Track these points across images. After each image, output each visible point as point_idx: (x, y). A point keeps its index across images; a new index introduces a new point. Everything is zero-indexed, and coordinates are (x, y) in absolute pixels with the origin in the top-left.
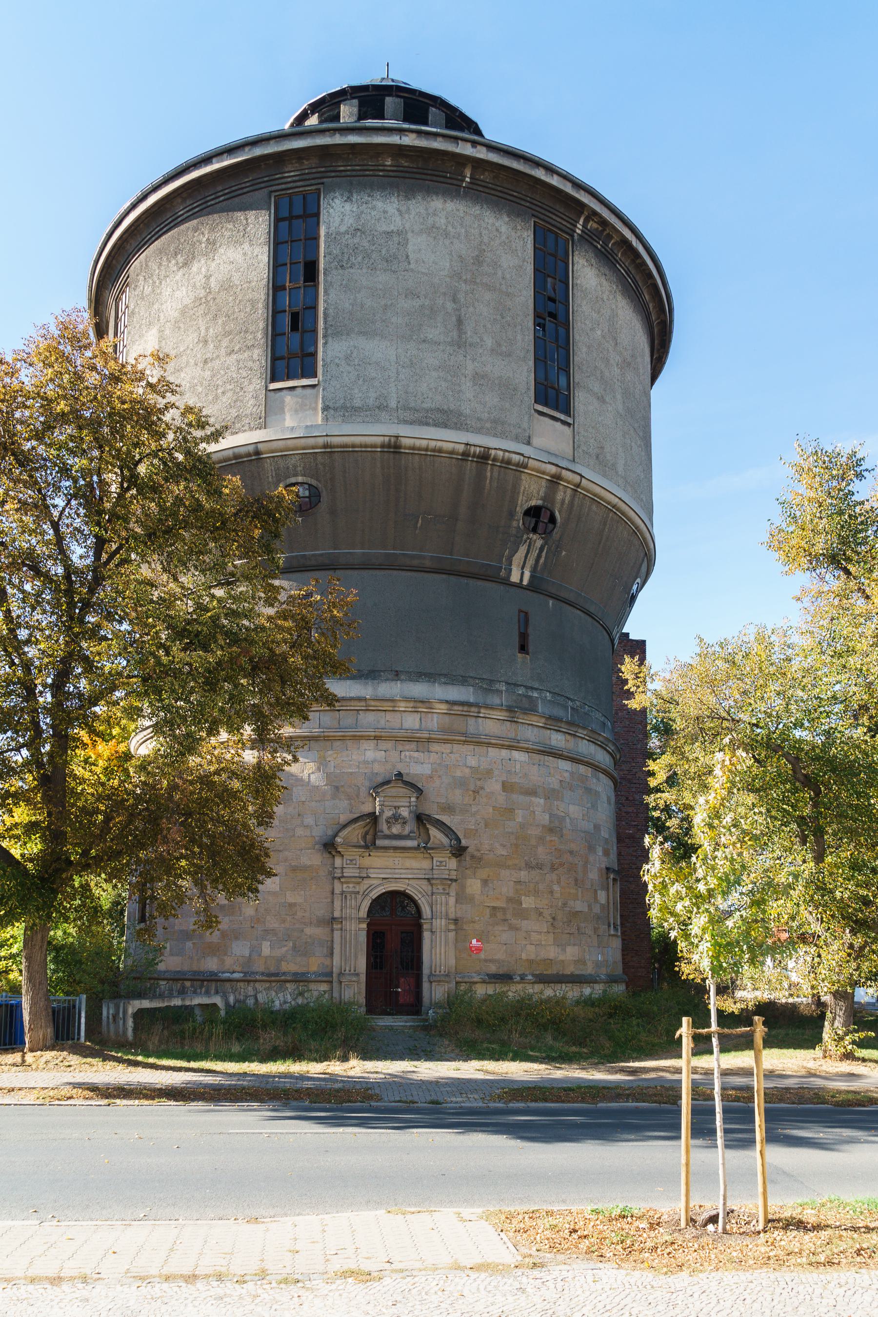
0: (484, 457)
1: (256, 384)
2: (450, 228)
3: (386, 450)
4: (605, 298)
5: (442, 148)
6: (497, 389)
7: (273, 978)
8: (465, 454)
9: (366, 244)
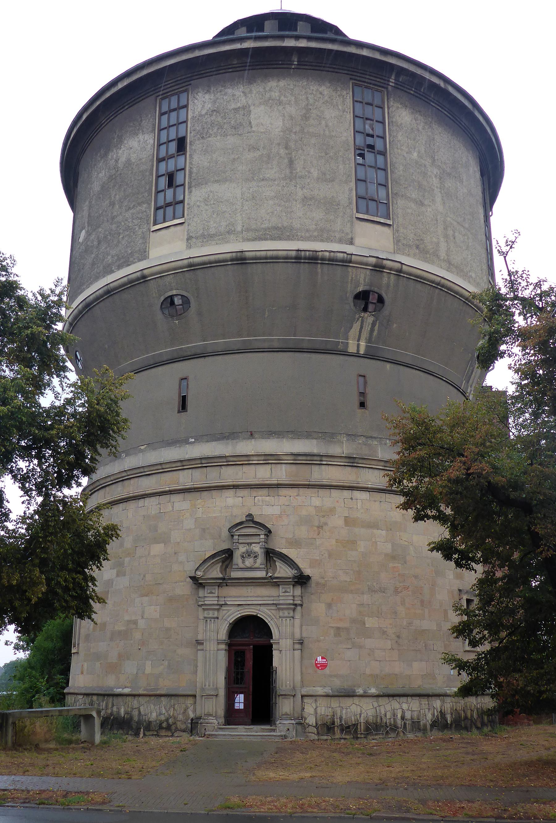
2: (282, 98)
9: (219, 119)
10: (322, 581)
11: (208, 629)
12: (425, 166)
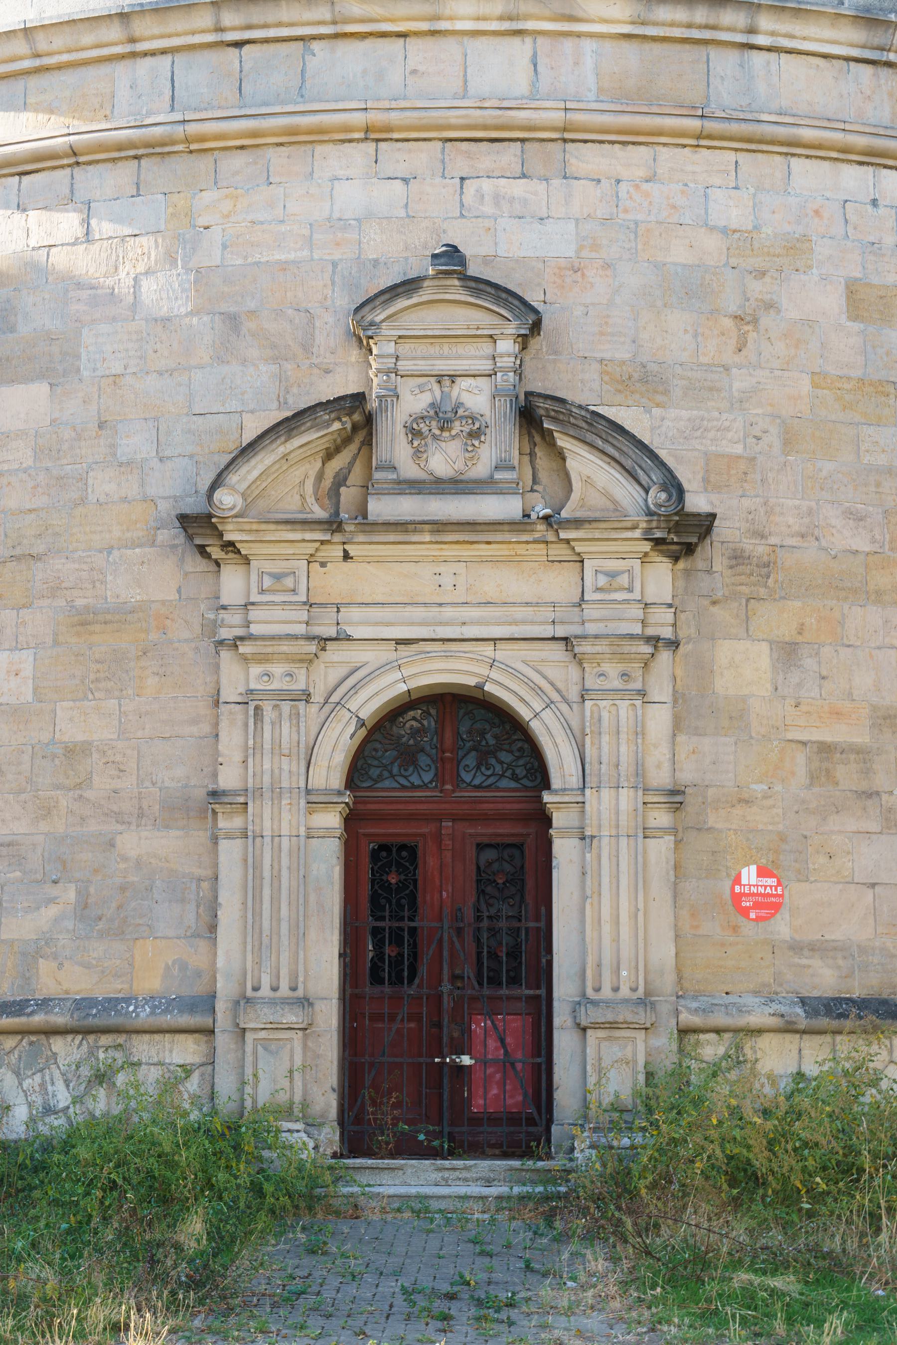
10: (760, 550)
11: (267, 746)
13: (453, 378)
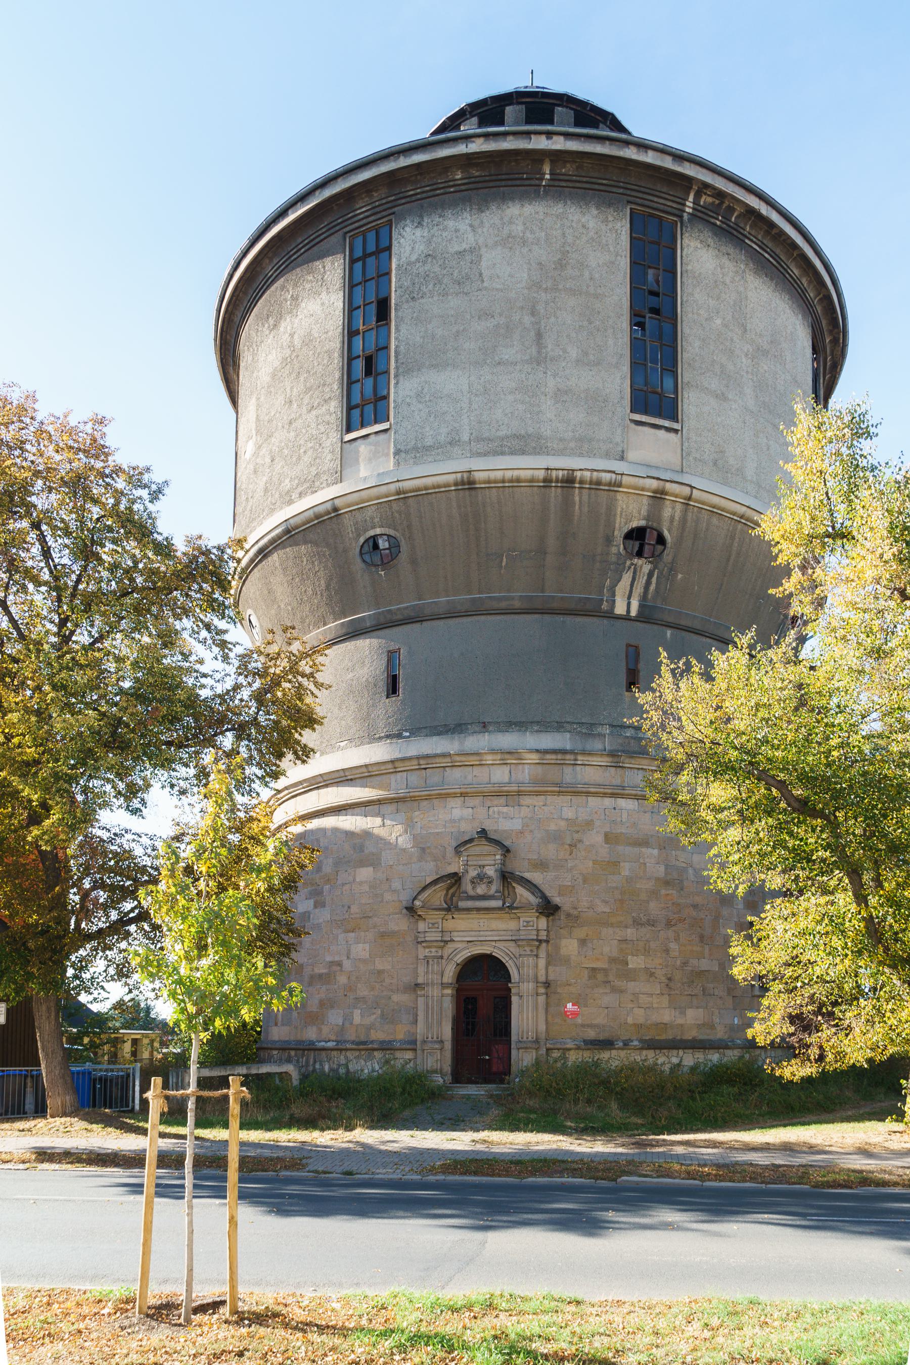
0: (569, 481)
1: (334, 437)
2: (528, 234)
3: (460, 487)
4: (728, 280)
5: (513, 147)
6: (582, 404)
7: (361, 1047)
8: (547, 480)
9: (437, 269)
10: (576, 913)
12: (732, 340)
13: (484, 866)
